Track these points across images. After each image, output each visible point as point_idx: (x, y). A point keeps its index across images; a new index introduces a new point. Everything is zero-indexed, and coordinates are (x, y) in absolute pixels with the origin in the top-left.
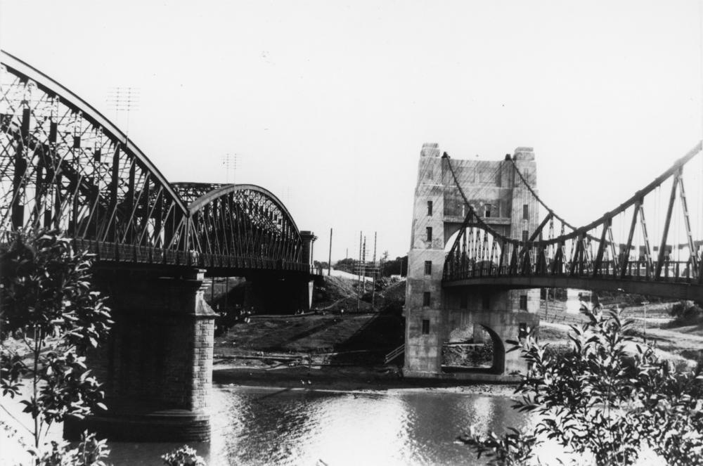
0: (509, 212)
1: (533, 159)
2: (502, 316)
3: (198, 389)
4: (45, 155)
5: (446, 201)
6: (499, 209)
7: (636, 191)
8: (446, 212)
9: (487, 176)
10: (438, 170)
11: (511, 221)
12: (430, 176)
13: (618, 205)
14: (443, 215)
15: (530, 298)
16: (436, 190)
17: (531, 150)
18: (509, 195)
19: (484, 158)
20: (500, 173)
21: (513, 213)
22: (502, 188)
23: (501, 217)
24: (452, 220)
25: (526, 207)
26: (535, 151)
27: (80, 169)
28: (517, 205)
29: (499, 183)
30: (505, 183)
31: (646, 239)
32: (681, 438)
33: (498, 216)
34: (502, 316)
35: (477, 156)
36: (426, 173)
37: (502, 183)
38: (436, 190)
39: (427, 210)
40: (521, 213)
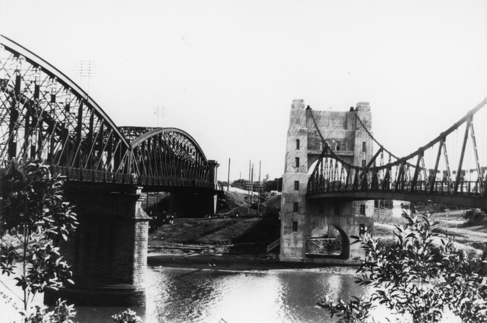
0: (352, 147)
1: (369, 110)
2: (348, 219)
3: (137, 269)
4: (31, 107)
5: (309, 140)
6: (345, 145)
7: (441, 132)
8: (309, 147)
9: (338, 122)
10: (303, 118)
11: (354, 153)
12: (298, 122)
13: (428, 142)
14: (307, 149)
15: (367, 206)
16: (302, 132)
17: (368, 104)
18: (353, 135)
19: (335, 109)
20: (347, 120)
21: (356, 147)
22: (347, 130)
23: (347, 151)
24: (313, 152)
25: (364, 143)
26: (370, 105)
27: (55, 117)
28: (358, 142)
29: (346, 127)
30: (350, 127)
31: (448, 166)
32: (472, 304)
33: (345, 150)
34: (348, 219)
35: (331, 108)
36: (295, 120)
37: (348, 127)
38: (302, 132)
39: (296, 146)
40: (361, 148)
